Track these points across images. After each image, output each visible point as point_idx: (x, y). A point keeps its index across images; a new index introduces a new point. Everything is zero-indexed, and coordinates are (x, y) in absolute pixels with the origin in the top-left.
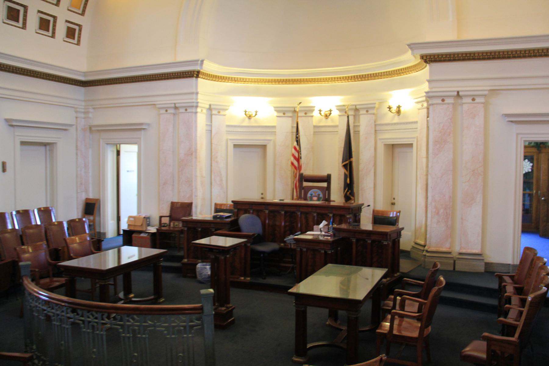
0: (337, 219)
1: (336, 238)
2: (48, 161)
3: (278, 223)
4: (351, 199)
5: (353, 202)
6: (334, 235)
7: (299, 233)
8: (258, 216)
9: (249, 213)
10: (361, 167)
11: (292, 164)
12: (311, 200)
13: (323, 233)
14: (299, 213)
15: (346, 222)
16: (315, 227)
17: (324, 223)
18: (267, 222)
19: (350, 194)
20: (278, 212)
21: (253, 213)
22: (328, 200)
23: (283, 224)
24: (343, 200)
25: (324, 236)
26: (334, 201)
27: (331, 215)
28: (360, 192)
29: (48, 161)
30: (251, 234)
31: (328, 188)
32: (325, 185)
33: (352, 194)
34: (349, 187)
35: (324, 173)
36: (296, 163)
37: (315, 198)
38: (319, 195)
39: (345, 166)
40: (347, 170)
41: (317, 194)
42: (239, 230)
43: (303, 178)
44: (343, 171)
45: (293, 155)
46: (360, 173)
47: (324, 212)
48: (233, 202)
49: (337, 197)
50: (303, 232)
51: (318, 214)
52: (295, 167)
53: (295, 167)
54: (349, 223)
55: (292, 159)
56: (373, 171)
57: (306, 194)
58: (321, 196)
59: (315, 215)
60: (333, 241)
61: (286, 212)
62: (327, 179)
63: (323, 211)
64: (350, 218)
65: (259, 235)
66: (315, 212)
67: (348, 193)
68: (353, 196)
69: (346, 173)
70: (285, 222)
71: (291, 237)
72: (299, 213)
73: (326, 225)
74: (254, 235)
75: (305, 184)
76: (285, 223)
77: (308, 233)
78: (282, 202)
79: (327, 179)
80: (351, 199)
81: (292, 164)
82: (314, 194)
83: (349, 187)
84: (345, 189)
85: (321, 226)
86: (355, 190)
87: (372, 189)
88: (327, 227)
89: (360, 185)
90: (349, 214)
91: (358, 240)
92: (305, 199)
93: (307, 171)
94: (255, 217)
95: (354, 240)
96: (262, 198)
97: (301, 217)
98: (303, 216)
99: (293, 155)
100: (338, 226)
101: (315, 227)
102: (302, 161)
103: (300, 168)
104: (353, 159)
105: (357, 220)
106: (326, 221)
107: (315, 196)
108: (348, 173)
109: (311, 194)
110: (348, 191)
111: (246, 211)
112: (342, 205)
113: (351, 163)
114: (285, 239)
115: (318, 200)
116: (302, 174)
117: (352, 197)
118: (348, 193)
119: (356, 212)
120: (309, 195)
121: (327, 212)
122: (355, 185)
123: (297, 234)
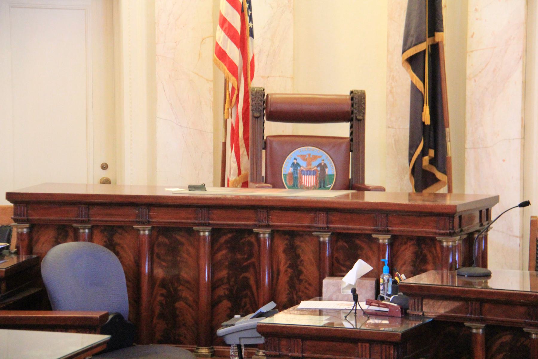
0: (407, 253)
1: (413, 324)
2: (243, 150)
3: (186, 274)
4: (436, 180)
5: (444, 190)
6: (405, 313)
7: (271, 305)
8: (111, 245)
9: (76, 238)
10: (474, 62)
11: (221, 54)
12: (296, 184)
13: (363, 305)
14: (265, 235)
15: (440, 263)
16: (328, 283)
17: (361, 267)
18: (147, 269)
19: (433, 162)
20: (189, 231)
21: (91, 239)
22: (354, 182)
23: (206, 275)
24: (406, 184)
25: (368, 314)
26: (381, 189)
27: (384, 239)
28: (470, 156)
29: (243, 150)
30: (97, 315)
31: (355, 143)
32: (342, 130)
33: (441, 161)
34: (431, 139)
35: (336, 87)
36: (233, 52)
37: (309, 180)
38: (323, 167)
39: (413, 62)
40: (423, 81)
41: (314, 164)
42: (42, 299)
43: (262, 109)
44: (406, 78)
45: (224, 22)
46: (470, 86)
47: (347, 233)
48: (10, 196)
49: (387, 176)
50: (291, 302)
51: (338, 236)
52: (232, 68)
53: (232, 68)
54: (452, 267)
55: (221, 36)
56: (517, 76)
57: (274, 167)
58: (331, 170)
59: (325, 238)
60: (406, 335)
61: (216, 232)
62: (352, 111)
63: (354, 227)
64: (452, 250)
65: (118, 316)
66: (328, 229)
67: (426, 159)
68: (445, 170)
69: (419, 85)
70: (214, 268)
71: (243, 322)
72: (265, 235)
73: (367, 276)
74: (105, 316)
75: (273, 128)
76: (213, 273)
77: (304, 304)
78: (198, 193)
79: (352, 111)
80: (436, 180)
81: (221, 54)
82: (303, 165)
83: (431, 139)
84: (413, 147)
85: (351, 277)
86: (452, 148)
87: (517, 144)
88: (371, 283)
89: (469, 129)
90: (451, 235)
91: (492, 331)
92: (277, 184)
93: (277, 81)
94: (97, 248)
95: (478, 330)
96: (106, 182)
97: (272, 249)
98: (281, 245)
99: (224, 22)
100: (413, 280)
101: (328, 283)
102: (255, 46)
103: (249, 68)
104: (446, 37)
105: (474, 253)
106: (367, 260)
107: (309, 172)
108: (424, 88)
109: (295, 166)
110: (424, 153)
111: (64, 232)
112: (404, 201)
113: (435, 50)
114: (221, 332)
115: (321, 184)
116: (261, 93)
117: (439, 175)
118: (426, 159)
119: (469, 231)
120: (287, 169)
121: (368, 228)
122: (451, 132)
123: (264, 309)
